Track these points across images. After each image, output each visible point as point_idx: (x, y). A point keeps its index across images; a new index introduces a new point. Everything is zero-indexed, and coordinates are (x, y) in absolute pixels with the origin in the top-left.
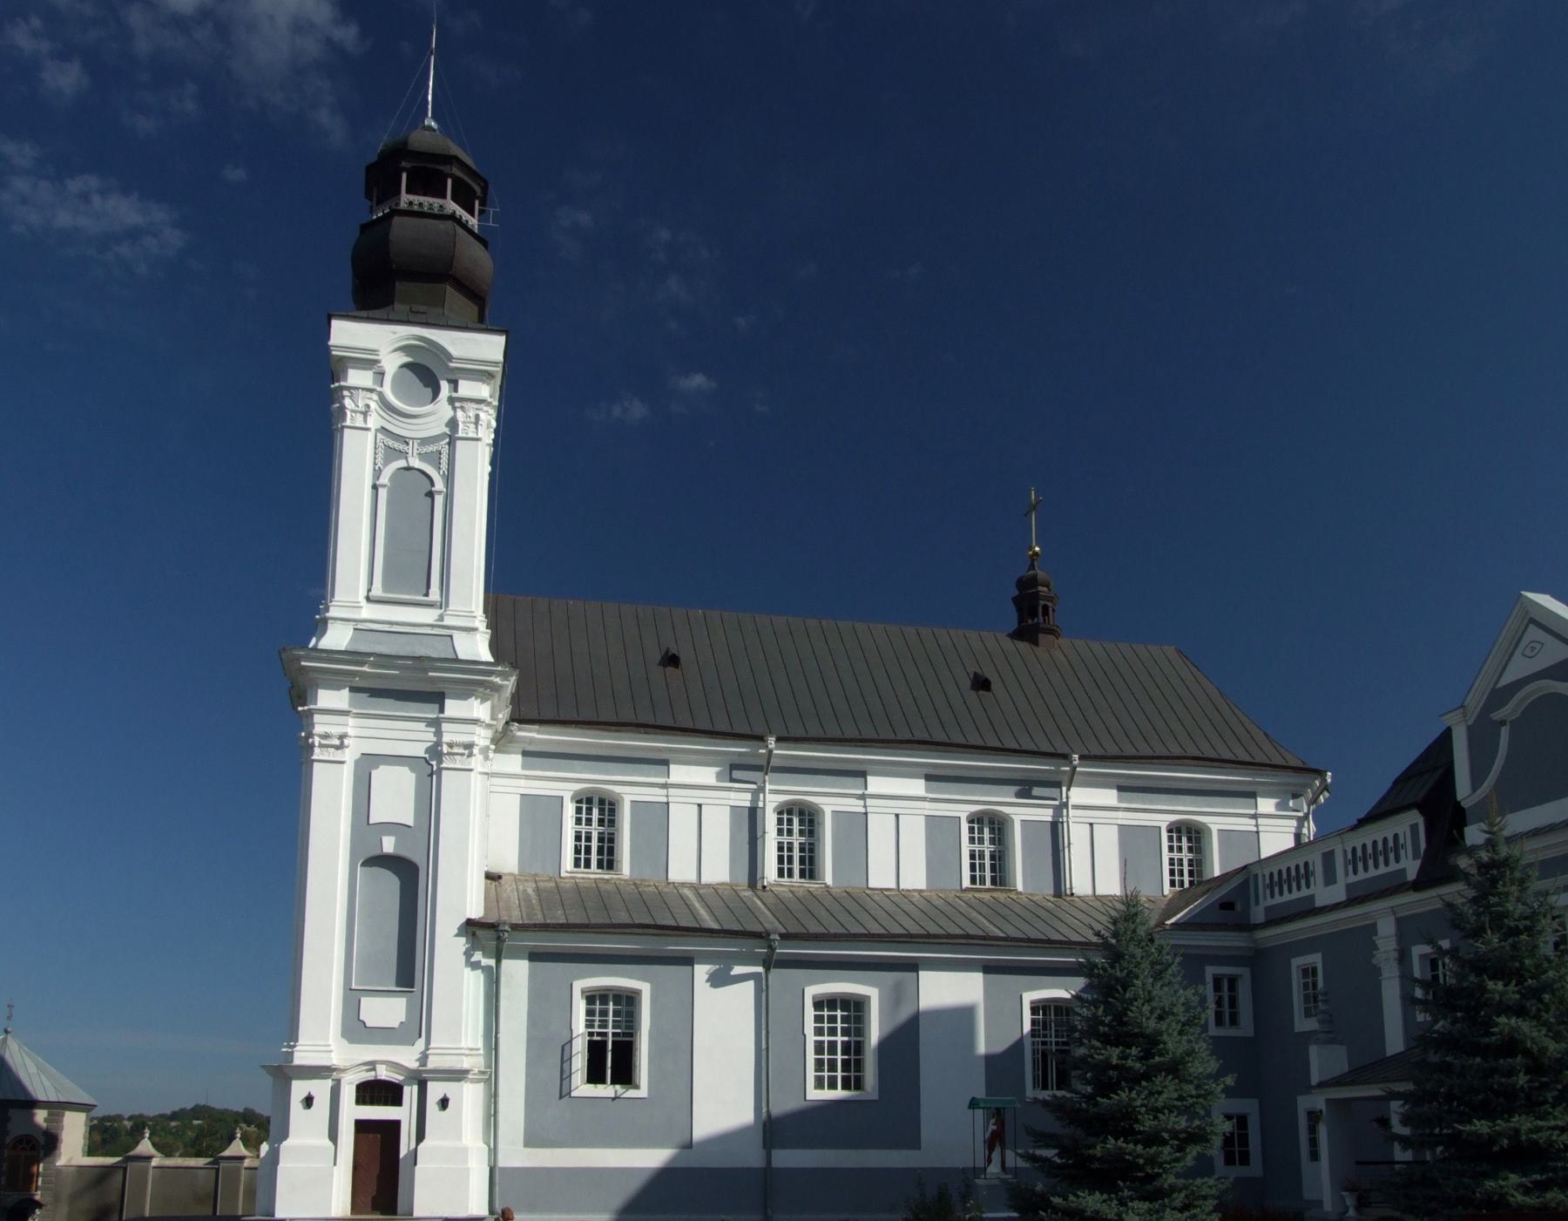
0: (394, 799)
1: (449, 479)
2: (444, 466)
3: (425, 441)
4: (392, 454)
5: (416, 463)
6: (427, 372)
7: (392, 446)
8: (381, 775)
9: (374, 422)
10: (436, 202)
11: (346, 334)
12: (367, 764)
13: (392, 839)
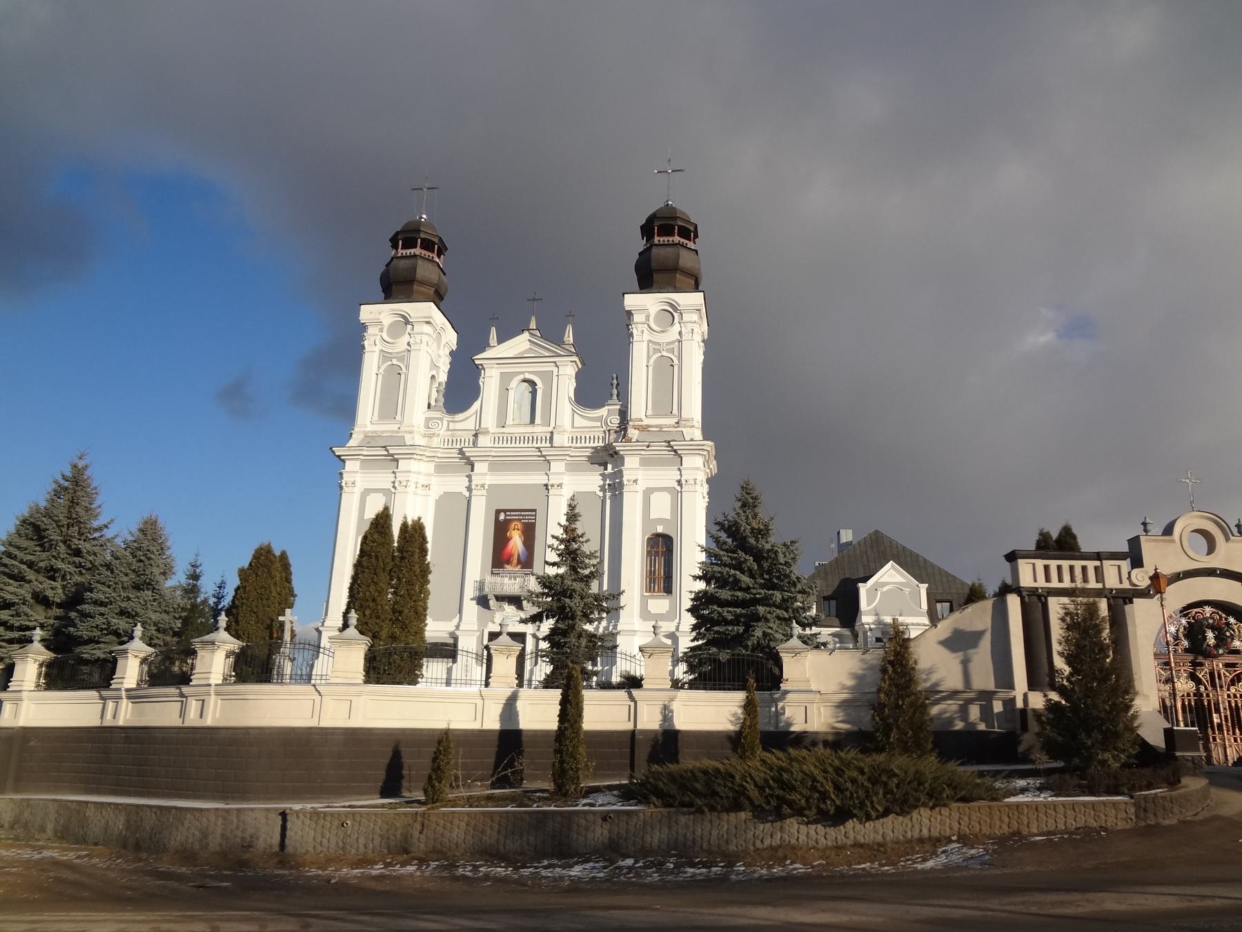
0: (661, 507)
1: (680, 358)
2: (676, 353)
3: (668, 344)
4: (656, 351)
5: (665, 354)
6: (672, 312)
7: (654, 346)
8: (655, 497)
9: (646, 336)
10: (671, 239)
11: (633, 301)
12: (648, 493)
13: (850, 532)
